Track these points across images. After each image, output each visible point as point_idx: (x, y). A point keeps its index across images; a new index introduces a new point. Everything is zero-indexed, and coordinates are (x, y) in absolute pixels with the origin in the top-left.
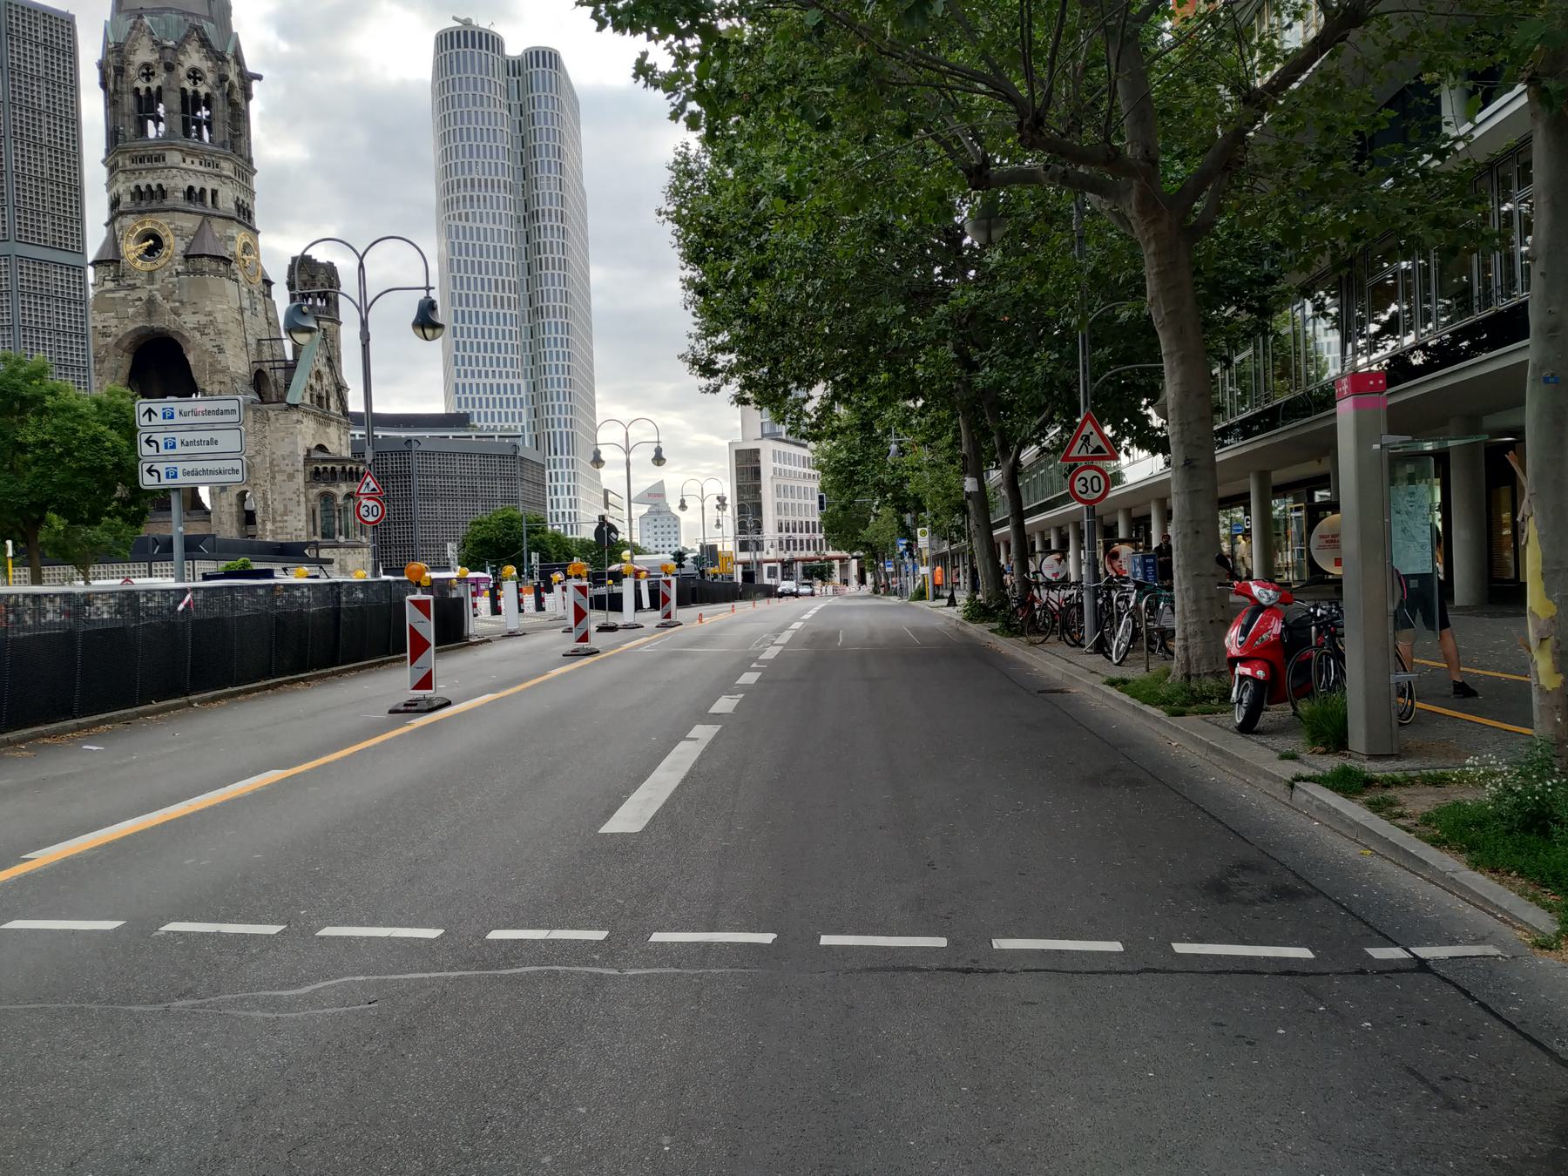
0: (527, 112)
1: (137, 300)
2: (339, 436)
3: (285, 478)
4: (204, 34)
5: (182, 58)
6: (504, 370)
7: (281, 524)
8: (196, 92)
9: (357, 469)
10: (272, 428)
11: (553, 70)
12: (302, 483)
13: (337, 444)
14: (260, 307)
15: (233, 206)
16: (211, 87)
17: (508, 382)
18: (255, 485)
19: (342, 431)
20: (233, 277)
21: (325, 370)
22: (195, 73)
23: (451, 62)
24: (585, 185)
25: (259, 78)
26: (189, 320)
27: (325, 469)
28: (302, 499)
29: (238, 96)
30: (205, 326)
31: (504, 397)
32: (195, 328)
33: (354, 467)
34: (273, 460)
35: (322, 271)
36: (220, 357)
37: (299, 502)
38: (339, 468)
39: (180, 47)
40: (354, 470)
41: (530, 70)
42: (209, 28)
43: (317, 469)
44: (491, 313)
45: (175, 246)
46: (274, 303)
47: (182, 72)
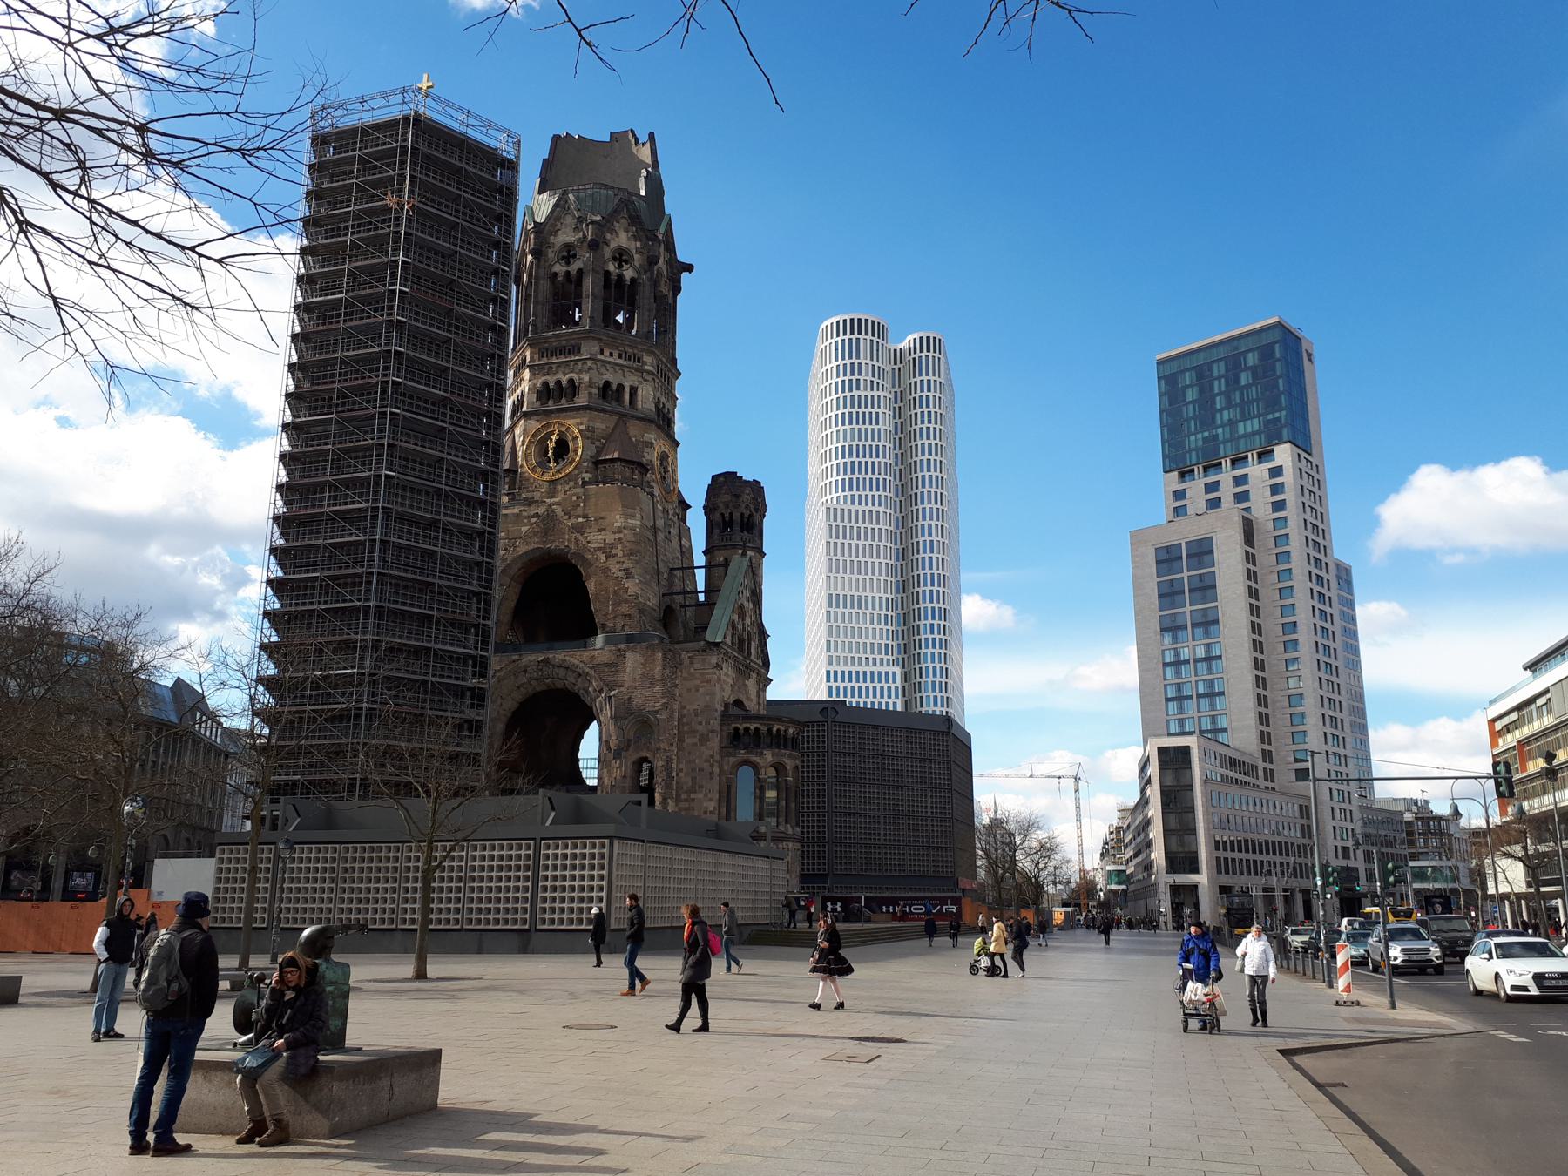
1: (532, 517)
3: (696, 740)
4: (635, 211)
5: (608, 236)
6: (878, 657)
7: (687, 805)
8: (620, 277)
9: (786, 731)
10: (685, 675)
12: (717, 749)
13: (755, 702)
14: (674, 531)
16: (638, 271)
17: (875, 669)
18: (658, 749)
21: (749, 606)
22: (621, 255)
23: (836, 350)
27: (747, 729)
28: (716, 770)
30: (612, 546)
31: (886, 686)
32: (599, 549)
33: (782, 728)
34: (684, 716)
35: (748, 490)
37: (712, 773)
38: (764, 729)
39: (604, 226)
43: (736, 729)
45: (580, 450)
47: (607, 252)
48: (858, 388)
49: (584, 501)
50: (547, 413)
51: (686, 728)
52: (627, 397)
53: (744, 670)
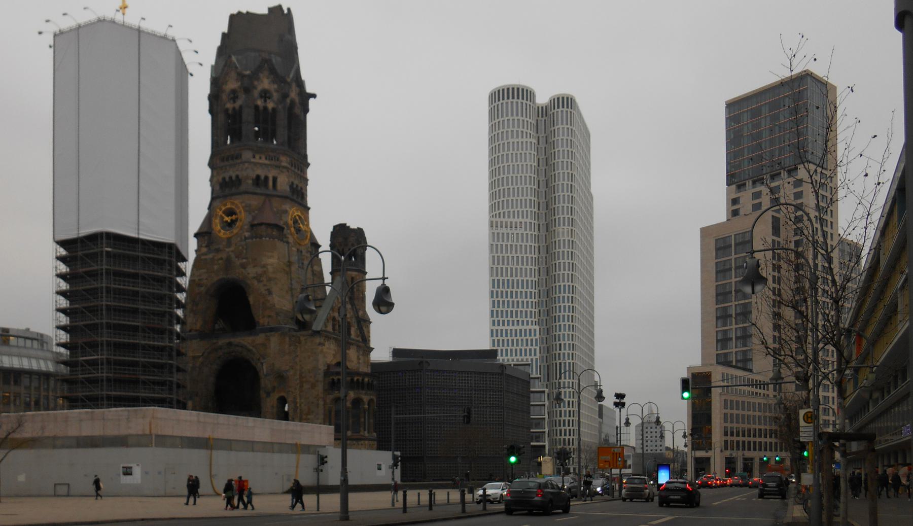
0: (550, 140)
2: (358, 356)
5: (256, 83)
8: (265, 108)
9: (363, 380)
11: (569, 110)
15: (288, 188)
18: (289, 391)
19: (361, 353)
20: (285, 240)
23: (498, 110)
24: (593, 190)
25: (314, 96)
26: (252, 271)
28: (321, 402)
29: (298, 110)
33: (360, 379)
36: (269, 298)
37: (318, 404)
39: (255, 76)
40: (360, 381)
41: (553, 111)
42: (276, 60)
43: (333, 379)
44: (518, 280)
45: (244, 217)
46: (320, 259)
47: (256, 93)
48: (512, 137)
49: (246, 249)
50: (225, 197)
51: (304, 380)
52: (271, 183)
53: (344, 344)
